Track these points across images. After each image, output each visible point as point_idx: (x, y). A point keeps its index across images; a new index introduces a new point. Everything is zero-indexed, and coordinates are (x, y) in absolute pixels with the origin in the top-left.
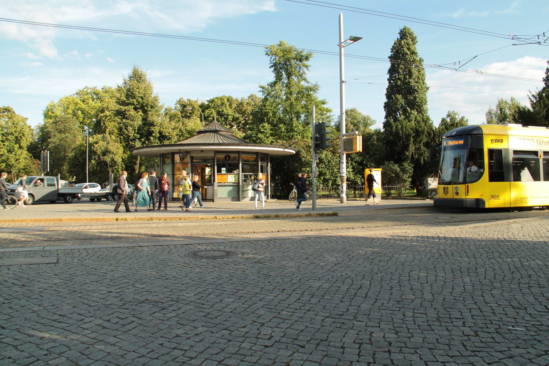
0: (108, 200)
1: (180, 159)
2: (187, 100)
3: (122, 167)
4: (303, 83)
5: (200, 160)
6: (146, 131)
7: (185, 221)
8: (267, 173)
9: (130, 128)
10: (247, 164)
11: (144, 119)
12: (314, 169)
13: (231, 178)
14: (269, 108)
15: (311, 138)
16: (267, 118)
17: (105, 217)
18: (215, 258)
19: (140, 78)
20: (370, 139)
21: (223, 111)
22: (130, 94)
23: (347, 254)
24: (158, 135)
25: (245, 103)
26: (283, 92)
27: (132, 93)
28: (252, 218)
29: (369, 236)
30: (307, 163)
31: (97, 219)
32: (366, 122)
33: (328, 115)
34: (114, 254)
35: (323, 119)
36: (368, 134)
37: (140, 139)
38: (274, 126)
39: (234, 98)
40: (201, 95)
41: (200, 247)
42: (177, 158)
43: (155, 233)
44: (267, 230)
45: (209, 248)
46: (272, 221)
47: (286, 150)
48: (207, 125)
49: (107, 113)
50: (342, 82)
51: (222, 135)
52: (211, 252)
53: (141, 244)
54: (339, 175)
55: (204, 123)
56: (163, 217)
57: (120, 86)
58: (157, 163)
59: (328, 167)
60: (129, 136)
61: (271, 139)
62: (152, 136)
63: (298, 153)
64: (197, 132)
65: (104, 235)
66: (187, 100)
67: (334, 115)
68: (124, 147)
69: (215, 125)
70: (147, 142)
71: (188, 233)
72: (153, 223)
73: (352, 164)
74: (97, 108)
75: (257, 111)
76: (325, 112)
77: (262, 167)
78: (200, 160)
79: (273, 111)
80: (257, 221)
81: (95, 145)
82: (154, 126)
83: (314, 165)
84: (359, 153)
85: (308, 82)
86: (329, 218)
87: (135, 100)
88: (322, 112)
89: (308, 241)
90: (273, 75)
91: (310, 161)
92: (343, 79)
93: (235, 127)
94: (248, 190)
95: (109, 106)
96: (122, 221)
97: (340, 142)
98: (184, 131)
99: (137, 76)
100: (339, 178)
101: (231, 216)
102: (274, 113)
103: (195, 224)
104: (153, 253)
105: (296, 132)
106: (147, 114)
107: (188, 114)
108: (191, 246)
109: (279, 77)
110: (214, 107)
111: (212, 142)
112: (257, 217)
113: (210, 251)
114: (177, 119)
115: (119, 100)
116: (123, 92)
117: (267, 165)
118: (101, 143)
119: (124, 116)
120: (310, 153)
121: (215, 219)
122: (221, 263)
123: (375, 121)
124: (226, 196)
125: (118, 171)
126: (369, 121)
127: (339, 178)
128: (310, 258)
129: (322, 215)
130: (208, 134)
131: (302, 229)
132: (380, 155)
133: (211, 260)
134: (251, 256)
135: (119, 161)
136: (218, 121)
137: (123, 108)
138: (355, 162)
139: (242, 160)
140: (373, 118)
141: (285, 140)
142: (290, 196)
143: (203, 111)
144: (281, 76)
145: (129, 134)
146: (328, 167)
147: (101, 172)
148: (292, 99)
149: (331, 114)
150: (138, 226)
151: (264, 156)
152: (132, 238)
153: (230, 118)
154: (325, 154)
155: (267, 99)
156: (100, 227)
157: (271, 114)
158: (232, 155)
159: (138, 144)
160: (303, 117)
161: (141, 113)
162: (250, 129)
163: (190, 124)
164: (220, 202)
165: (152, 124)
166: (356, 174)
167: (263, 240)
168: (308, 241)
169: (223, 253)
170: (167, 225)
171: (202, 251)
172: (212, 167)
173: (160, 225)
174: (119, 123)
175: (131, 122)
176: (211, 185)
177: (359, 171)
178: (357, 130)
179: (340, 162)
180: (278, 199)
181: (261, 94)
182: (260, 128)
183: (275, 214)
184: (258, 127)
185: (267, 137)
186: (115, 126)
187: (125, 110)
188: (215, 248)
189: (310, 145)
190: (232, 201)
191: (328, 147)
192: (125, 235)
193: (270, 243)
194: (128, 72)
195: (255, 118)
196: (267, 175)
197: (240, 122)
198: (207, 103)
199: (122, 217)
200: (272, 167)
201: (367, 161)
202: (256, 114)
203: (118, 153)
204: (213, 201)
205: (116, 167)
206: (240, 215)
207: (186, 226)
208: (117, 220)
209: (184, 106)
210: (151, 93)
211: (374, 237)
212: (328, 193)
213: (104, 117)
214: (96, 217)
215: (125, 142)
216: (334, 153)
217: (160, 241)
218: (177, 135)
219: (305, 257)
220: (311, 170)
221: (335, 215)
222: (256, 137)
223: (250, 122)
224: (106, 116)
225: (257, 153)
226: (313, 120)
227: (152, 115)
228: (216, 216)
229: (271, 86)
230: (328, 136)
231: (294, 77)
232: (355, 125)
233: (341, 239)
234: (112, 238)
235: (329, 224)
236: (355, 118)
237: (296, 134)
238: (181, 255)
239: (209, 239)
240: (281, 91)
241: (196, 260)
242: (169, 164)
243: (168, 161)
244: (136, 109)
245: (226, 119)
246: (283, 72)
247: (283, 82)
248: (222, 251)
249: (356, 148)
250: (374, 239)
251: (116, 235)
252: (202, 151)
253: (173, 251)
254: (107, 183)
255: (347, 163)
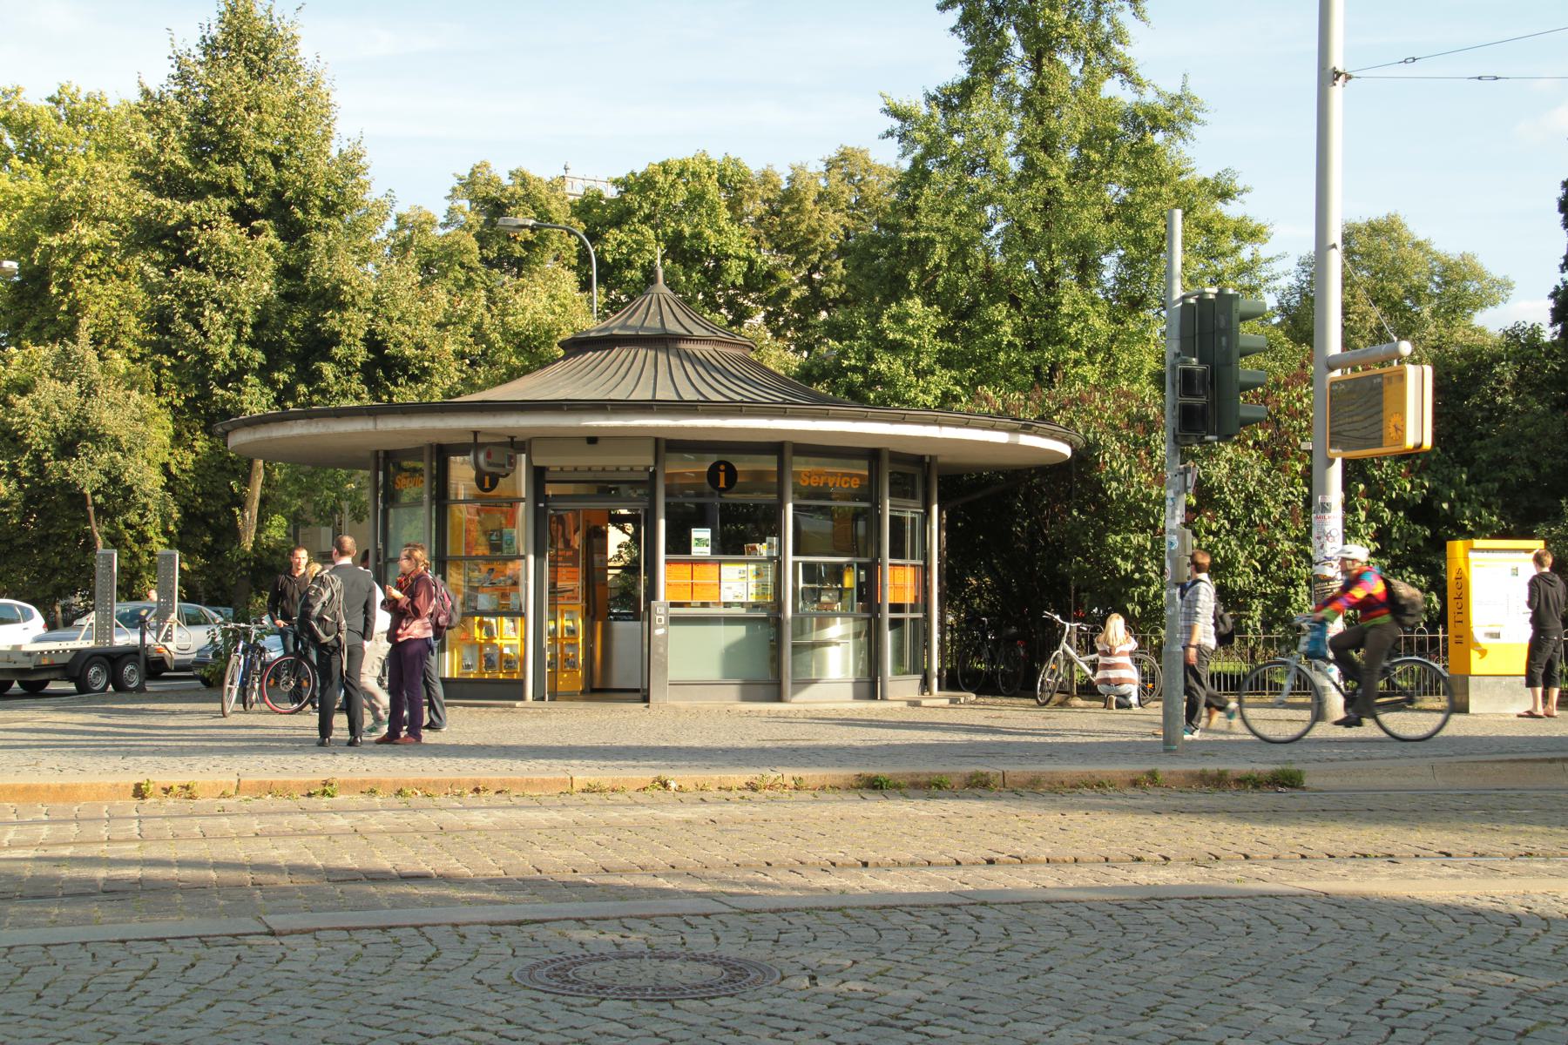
0: (83, 688)
1: (480, 481)
2: (512, 175)
3: (166, 518)
4: (1112, 89)
5: (582, 489)
6: (298, 333)
7: (502, 800)
8: (926, 556)
9: (213, 318)
10: (820, 509)
11: (289, 272)
12: (1172, 541)
13: (738, 582)
14: (935, 220)
15: (1158, 379)
16: (924, 274)
17: (70, 778)
18: (666, 995)
19: (265, 50)
20: (1477, 381)
21: (698, 236)
22: (211, 136)
23: (1371, 997)
24: (362, 355)
25: (812, 196)
26: (1009, 137)
27: (220, 130)
28: (850, 788)
29: (1485, 904)
30: (1133, 509)
31: (27, 789)
32: (1458, 289)
33: (1245, 254)
34: (130, 976)
35: (1217, 279)
36: (1469, 354)
37: (264, 373)
38: (962, 316)
39: (754, 166)
40: (585, 148)
41: (587, 935)
42: (462, 473)
43: (348, 861)
44: (932, 855)
45: (635, 940)
46: (951, 806)
47: (1026, 440)
48: (613, 306)
49: (85, 233)
50: (1328, 76)
51: (693, 359)
52: (645, 963)
53: (276, 922)
54: (1303, 571)
55: (598, 295)
56: (389, 778)
57: (154, 89)
58: (353, 497)
59: (1246, 526)
60: (206, 358)
61: (943, 379)
62: (331, 359)
63: (1085, 457)
64: (562, 345)
65: (65, 873)
66: (512, 175)
67: (1282, 253)
68: (176, 412)
69: (661, 310)
70: (302, 388)
71: (521, 864)
72: (335, 811)
73: (1372, 516)
74: (28, 202)
75: (874, 239)
76: (1229, 243)
77: (897, 524)
78: (582, 489)
79: (956, 239)
80: (879, 808)
81: (12, 397)
82: (342, 306)
83: (1174, 519)
84: (1413, 460)
85: (1137, 83)
86: (1255, 797)
87: (237, 171)
88: (1212, 239)
89: (1153, 916)
90: (958, 47)
91: (1147, 498)
92: (1337, 62)
93: (759, 318)
94: (826, 644)
95: (95, 193)
96: (170, 801)
97: (1312, 400)
98: (495, 336)
99: (246, 46)
100: (1303, 589)
101: (739, 776)
102: (960, 251)
103: (553, 814)
104: (340, 967)
105: (1075, 345)
106: (305, 245)
107: (518, 250)
108: (544, 933)
109: (986, 59)
110: (647, 218)
111: (642, 394)
112: (874, 785)
113: (640, 956)
114: (461, 275)
115: (155, 163)
116: (175, 122)
117: (928, 513)
118: (48, 389)
119: (180, 252)
120: (1150, 454)
121: (660, 794)
122: (701, 1020)
123: (1507, 285)
124: (714, 673)
125: (143, 539)
126: (1473, 287)
127: (1303, 589)
128: (1166, 1010)
129: (1218, 781)
130: (621, 354)
131: (1113, 851)
132: (1535, 466)
133: (647, 1008)
134: (859, 986)
135: (147, 486)
136: (673, 285)
137: (176, 210)
138: (1393, 505)
139: (797, 491)
140: (1493, 265)
141: (1015, 387)
142: (1045, 677)
143: (594, 237)
144: (999, 52)
145: (211, 349)
146: (1246, 526)
147: (44, 540)
148: (1053, 171)
149: (1264, 251)
150: (256, 824)
151: (911, 471)
152: (220, 886)
153: (735, 271)
154: (1229, 463)
155: (926, 175)
156: (45, 831)
157: (939, 254)
158: (743, 465)
159: (255, 399)
160: (1110, 267)
161: (270, 237)
162: (834, 330)
163: (522, 300)
164: (682, 704)
165: (331, 298)
166: (1397, 566)
167: (914, 907)
168: (1153, 916)
169: (711, 972)
170: (406, 818)
171: (603, 958)
172: (643, 522)
173: (374, 822)
174: (151, 290)
175: (220, 287)
176: (636, 616)
177: (1416, 549)
178: (1404, 334)
179: (1308, 501)
180: (979, 693)
181: (893, 144)
182: (885, 322)
183: (969, 769)
184: (874, 318)
185: (920, 374)
186: (126, 303)
187: (187, 222)
188: (663, 942)
189: (1153, 411)
190: (746, 697)
191: (1245, 423)
192: (188, 873)
193: (953, 922)
194: (195, 16)
195: (863, 270)
196: (926, 569)
197: (784, 293)
198: (611, 193)
199: (166, 780)
200: (949, 527)
201: (1462, 498)
202: (866, 249)
203: (143, 442)
204: (646, 699)
205: (133, 517)
206: (788, 774)
207: (510, 828)
208: (139, 792)
209: (495, 207)
210: (326, 138)
211: (1518, 910)
212: (1245, 668)
213: (64, 250)
214: (22, 780)
215: (183, 385)
216: (1276, 454)
217: (372, 905)
218: (461, 355)
219: (1141, 1001)
220: (1158, 543)
221: (1287, 781)
222: (864, 371)
223: (833, 291)
224: (79, 252)
225: (873, 455)
226: (1170, 284)
227: (330, 251)
228: (666, 774)
229: (947, 107)
230: (1246, 367)
231: (1065, 59)
232: (1393, 308)
233: (1331, 912)
234: (114, 892)
235: (1260, 830)
236: (1397, 272)
237: (1073, 355)
238: (487, 977)
239: (634, 893)
240: (999, 130)
241: (570, 1009)
242: (417, 502)
243: (415, 489)
244: (243, 216)
245: (714, 276)
246: (1011, 33)
247: (1009, 86)
248: (704, 959)
249: (1400, 430)
250: (1517, 920)
251: (134, 873)
252: (592, 440)
253: (447, 956)
254: (77, 600)
255: (1348, 508)
